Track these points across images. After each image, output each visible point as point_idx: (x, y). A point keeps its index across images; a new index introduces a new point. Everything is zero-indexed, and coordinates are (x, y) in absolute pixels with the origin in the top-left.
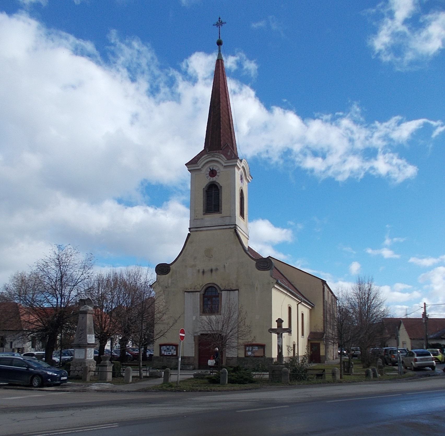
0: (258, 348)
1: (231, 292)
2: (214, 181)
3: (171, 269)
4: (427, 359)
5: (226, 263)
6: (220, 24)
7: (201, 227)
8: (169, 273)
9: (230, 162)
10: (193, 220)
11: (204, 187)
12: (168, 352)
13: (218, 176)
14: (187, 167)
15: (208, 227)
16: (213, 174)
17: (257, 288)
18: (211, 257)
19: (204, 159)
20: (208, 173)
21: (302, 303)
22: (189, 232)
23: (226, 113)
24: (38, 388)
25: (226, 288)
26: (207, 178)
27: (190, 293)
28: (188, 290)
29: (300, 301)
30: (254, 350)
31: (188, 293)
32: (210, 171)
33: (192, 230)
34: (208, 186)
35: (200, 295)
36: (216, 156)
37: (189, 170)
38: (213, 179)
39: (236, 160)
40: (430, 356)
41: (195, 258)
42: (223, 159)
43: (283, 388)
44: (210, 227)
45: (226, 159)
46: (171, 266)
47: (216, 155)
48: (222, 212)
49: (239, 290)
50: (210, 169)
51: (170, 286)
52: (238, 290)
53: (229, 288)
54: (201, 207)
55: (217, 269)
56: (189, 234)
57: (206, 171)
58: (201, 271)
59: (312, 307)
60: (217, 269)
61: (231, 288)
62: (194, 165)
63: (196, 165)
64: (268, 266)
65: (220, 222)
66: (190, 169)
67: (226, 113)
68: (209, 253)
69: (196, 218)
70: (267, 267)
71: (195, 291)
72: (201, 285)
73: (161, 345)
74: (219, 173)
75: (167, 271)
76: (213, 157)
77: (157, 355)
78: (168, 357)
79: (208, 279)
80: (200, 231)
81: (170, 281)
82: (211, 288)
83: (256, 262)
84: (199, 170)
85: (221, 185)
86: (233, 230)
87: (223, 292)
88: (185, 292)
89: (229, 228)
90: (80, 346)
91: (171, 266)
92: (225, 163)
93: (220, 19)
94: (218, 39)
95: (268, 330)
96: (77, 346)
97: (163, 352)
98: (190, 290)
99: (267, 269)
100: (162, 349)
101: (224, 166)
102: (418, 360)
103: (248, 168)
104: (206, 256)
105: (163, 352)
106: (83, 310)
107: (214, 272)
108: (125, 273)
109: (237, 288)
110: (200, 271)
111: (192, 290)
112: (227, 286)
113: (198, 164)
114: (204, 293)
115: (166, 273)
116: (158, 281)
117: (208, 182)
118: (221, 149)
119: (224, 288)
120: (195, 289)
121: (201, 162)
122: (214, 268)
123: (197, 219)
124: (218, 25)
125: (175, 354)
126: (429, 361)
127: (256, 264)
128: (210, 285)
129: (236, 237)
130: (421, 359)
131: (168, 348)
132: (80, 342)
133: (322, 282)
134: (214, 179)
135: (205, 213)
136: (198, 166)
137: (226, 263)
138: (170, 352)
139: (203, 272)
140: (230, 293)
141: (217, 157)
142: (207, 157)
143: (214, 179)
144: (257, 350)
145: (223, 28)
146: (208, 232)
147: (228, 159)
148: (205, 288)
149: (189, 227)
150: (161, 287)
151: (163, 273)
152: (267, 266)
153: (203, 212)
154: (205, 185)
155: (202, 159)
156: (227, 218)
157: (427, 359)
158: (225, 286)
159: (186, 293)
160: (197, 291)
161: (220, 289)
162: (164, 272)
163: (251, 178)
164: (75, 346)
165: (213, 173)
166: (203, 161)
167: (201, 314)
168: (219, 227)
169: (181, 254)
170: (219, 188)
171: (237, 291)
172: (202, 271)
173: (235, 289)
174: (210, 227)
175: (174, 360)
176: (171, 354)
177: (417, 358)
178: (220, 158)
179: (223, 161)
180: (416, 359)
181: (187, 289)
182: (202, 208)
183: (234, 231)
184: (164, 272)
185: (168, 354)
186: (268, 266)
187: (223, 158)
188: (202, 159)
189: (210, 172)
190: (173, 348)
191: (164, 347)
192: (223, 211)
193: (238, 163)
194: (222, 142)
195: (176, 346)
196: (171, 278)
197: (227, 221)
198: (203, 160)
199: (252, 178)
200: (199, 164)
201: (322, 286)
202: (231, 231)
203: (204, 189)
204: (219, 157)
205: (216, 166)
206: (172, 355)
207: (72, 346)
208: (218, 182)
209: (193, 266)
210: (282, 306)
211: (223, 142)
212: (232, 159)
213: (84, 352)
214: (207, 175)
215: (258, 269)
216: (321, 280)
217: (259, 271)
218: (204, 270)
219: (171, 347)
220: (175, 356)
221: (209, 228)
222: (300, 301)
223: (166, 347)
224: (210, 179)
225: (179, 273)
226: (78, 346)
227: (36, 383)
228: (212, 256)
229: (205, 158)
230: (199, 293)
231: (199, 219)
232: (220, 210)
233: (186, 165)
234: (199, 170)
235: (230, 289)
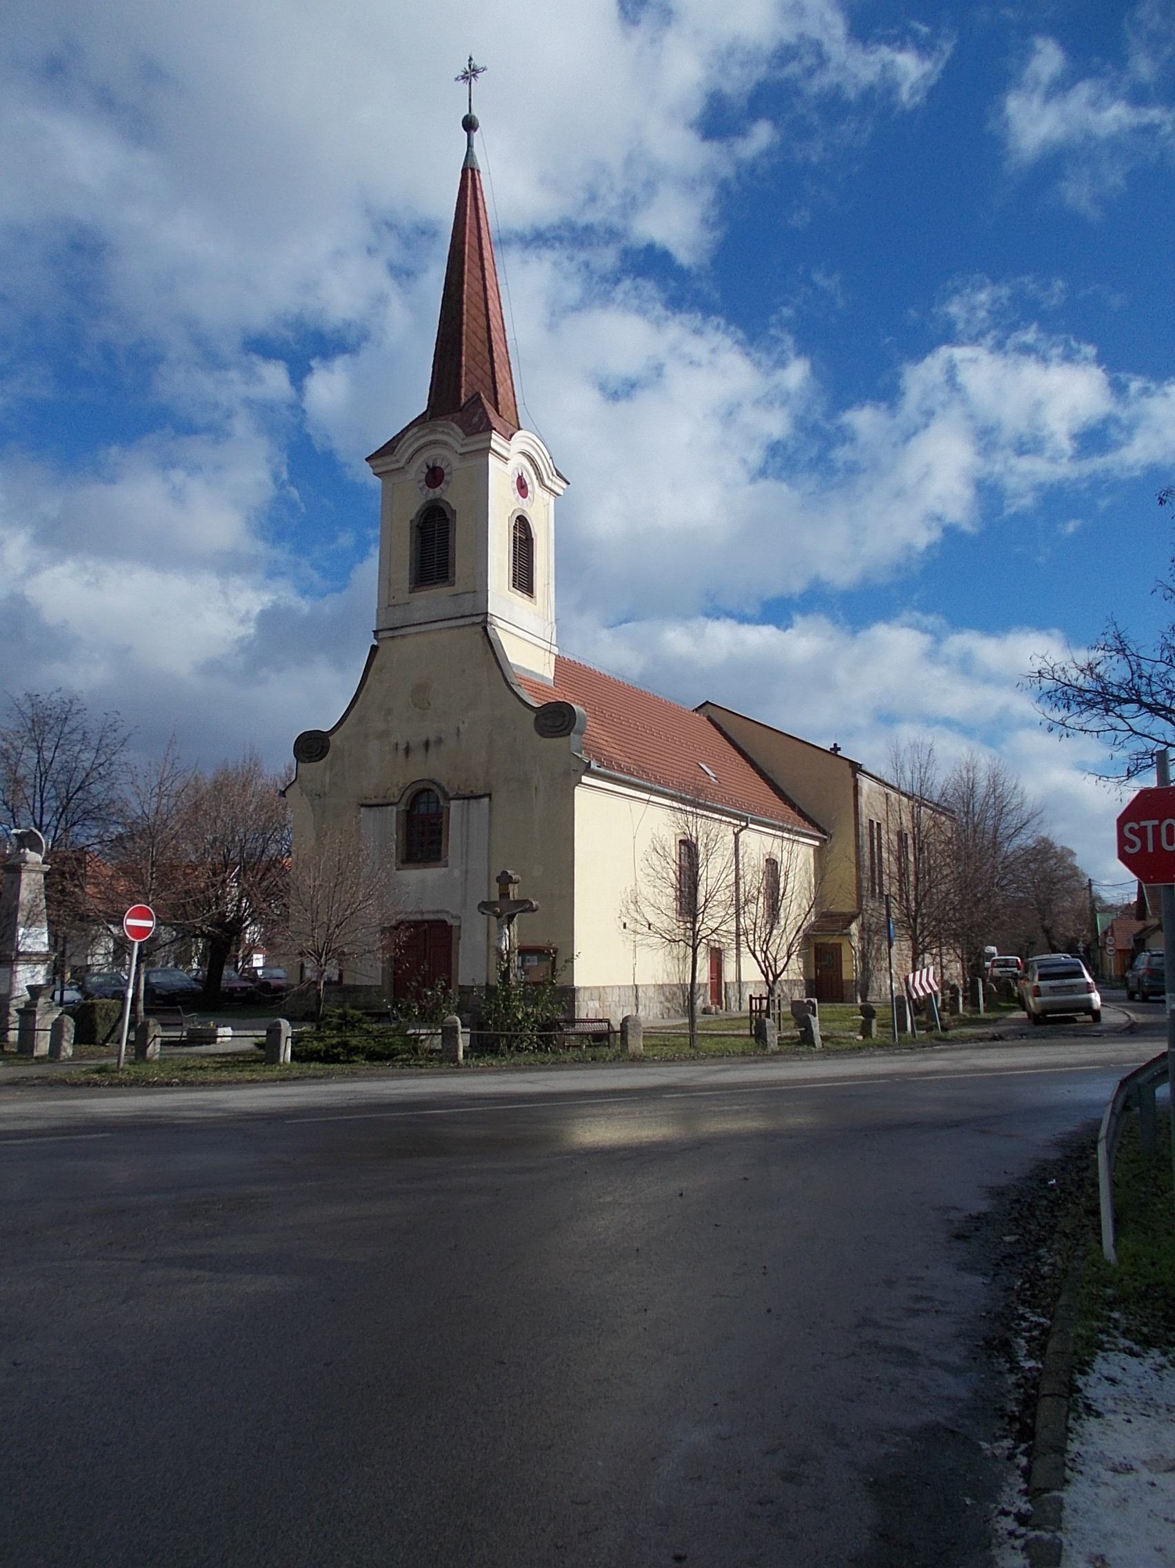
0: (539, 960)
1: (472, 801)
4: (1071, 989)
5: (463, 722)
6: (471, 73)
7: (402, 627)
9: (477, 442)
10: (386, 608)
11: (412, 516)
14: (372, 467)
15: (420, 624)
17: (536, 789)
19: (412, 439)
20: (423, 476)
21: (751, 826)
22: (376, 643)
23: (480, 311)
25: (460, 793)
27: (372, 808)
28: (368, 802)
29: (744, 824)
30: (528, 964)
31: (368, 809)
32: (426, 471)
33: (381, 635)
35: (398, 812)
37: (375, 474)
38: (435, 492)
40: (1081, 980)
43: (428, 1074)
45: (463, 435)
46: (331, 738)
48: (456, 581)
49: (493, 796)
50: (428, 467)
52: (489, 795)
53: (467, 792)
54: (404, 574)
55: (440, 741)
56: (374, 649)
57: (417, 471)
58: (402, 747)
59: (823, 841)
60: (440, 741)
61: (472, 792)
63: (394, 459)
64: (566, 723)
66: (378, 470)
67: (480, 311)
68: (421, 697)
69: (393, 602)
70: (564, 726)
71: (386, 801)
72: (400, 786)
75: (322, 751)
76: (433, 431)
79: (419, 769)
80: (402, 636)
82: (426, 793)
83: (535, 715)
86: (480, 629)
87: (452, 802)
88: (362, 806)
89: (469, 625)
91: (331, 738)
92: (463, 446)
93: (471, 59)
94: (468, 112)
95: (476, 906)
98: (374, 801)
99: (561, 733)
101: (461, 454)
102: (1042, 989)
103: (548, 457)
104: (416, 705)
107: (432, 749)
108: (968, 784)
109: (487, 792)
110: (399, 746)
111: (379, 801)
112: (462, 787)
114: (408, 808)
115: (319, 757)
117: (423, 501)
118: (461, 410)
119: (455, 793)
120: (385, 797)
122: (432, 738)
124: (468, 78)
126: (1076, 994)
127: (536, 719)
128: (421, 786)
133: (850, 767)
136: (398, 461)
137: (463, 722)
139: (407, 751)
140: (468, 804)
142: (419, 435)
145: (478, 84)
148: (408, 792)
149: (375, 629)
150: (307, 795)
152: (563, 723)
153: (410, 584)
154: (415, 511)
157: (1071, 989)
158: (459, 788)
159: (363, 809)
160: (390, 802)
161: (445, 794)
162: (314, 754)
163: (564, 485)
165: (435, 476)
166: (410, 445)
167: (441, 863)
169: (356, 702)
170: (449, 516)
171: (486, 800)
172: (404, 747)
173: (483, 792)
177: (1042, 983)
178: (448, 434)
181: (366, 798)
182: (408, 573)
183: (481, 630)
186: (566, 723)
187: (455, 432)
189: (428, 473)
193: (495, 441)
194: (463, 390)
199: (568, 483)
201: (852, 780)
204: (446, 430)
208: (447, 500)
209: (384, 735)
210: (634, 837)
211: (466, 390)
212: (480, 432)
213: (8, 975)
215: (541, 735)
216: (847, 763)
217: (543, 739)
218: (408, 744)
221: (422, 628)
222: (744, 824)
224: (428, 492)
228: (429, 704)
230: (395, 808)
232: (450, 575)
233: (367, 460)
235: (470, 795)
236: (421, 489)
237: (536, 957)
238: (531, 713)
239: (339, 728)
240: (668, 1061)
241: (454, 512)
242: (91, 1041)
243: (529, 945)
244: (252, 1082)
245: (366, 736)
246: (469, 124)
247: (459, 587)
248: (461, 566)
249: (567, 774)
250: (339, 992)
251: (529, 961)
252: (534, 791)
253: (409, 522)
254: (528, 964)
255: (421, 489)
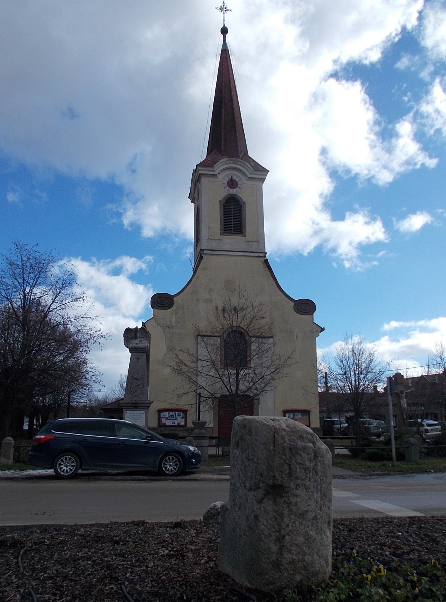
0: (302, 415)
2: (235, 195)
3: (175, 302)
8: (172, 308)
9: (258, 174)
12: (171, 421)
13: (240, 188)
15: (230, 251)
16: (232, 185)
17: (297, 337)
18: (234, 290)
24: (175, 478)
26: (225, 189)
30: (296, 417)
34: (226, 198)
36: (240, 163)
39: (264, 173)
41: (211, 290)
42: (249, 168)
44: (232, 251)
45: (253, 170)
47: (240, 162)
51: (174, 325)
62: (210, 169)
63: (213, 169)
65: (244, 247)
73: (160, 411)
74: (241, 184)
76: (234, 163)
77: (154, 426)
78: (172, 428)
81: (174, 319)
84: (215, 176)
85: (244, 201)
90: (138, 405)
93: (224, 3)
96: (131, 406)
97: (164, 421)
98: (204, 333)
100: (162, 417)
105: (164, 421)
106: (138, 345)
109: (271, 335)
113: (214, 168)
116: (155, 317)
121: (219, 165)
123: (212, 239)
125: (183, 423)
127: (294, 305)
129: (267, 270)
130: (432, 429)
131: (171, 416)
132: (136, 398)
134: (235, 191)
135: (223, 233)
136: (214, 171)
138: (176, 421)
141: (240, 165)
143: (235, 191)
144: (300, 417)
145: (227, 14)
146: (228, 258)
147: (255, 170)
150: (160, 326)
151: (163, 307)
155: (220, 163)
156: (254, 243)
162: (165, 305)
164: (128, 405)
166: (221, 166)
168: (245, 253)
169: (190, 283)
174: (232, 251)
175: (182, 432)
176: (176, 424)
177: (428, 428)
179: (248, 171)
180: (427, 429)
184: (165, 305)
185: (171, 424)
188: (220, 163)
190: (180, 416)
191: (164, 413)
192: (247, 233)
195: (185, 412)
196: (176, 315)
197: (254, 248)
198: (221, 164)
200: (216, 168)
202: (259, 261)
203: (220, 201)
205: (237, 177)
206: (179, 426)
207: (121, 405)
208: (240, 196)
213: (144, 416)
214: (225, 185)
219: (177, 413)
220: (182, 426)
223: (169, 414)
225: (187, 308)
226: (134, 405)
227: (170, 467)
228: (235, 289)
229: (224, 163)
231: (216, 240)
234: (215, 176)
236: (225, 187)
237: (300, 414)
238: (292, 302)
239: (180, 294)
240: (374, 457)
241: (244, 203)
242: (209, 457)
243: (296, 408)
244: (144, 480)
245: (198, 300)
246: (224, 31)
247: (248, 238)
248: (249, 228)
249: (312, 332)
250: (186, 431)
251: (297, 416)
252: (296, 338)
253: (218, 202)
254: (296, 417)
255: (225, 187)
